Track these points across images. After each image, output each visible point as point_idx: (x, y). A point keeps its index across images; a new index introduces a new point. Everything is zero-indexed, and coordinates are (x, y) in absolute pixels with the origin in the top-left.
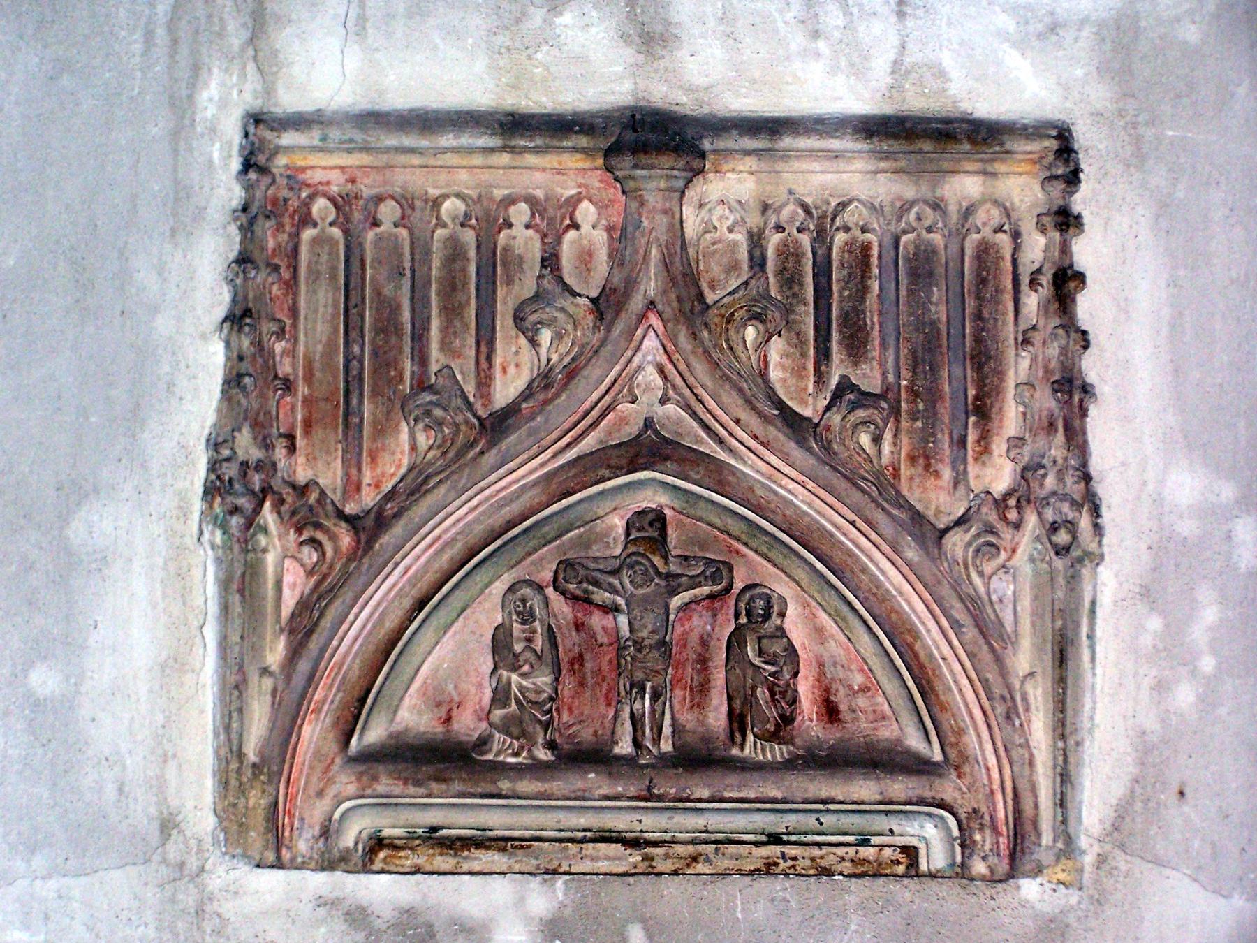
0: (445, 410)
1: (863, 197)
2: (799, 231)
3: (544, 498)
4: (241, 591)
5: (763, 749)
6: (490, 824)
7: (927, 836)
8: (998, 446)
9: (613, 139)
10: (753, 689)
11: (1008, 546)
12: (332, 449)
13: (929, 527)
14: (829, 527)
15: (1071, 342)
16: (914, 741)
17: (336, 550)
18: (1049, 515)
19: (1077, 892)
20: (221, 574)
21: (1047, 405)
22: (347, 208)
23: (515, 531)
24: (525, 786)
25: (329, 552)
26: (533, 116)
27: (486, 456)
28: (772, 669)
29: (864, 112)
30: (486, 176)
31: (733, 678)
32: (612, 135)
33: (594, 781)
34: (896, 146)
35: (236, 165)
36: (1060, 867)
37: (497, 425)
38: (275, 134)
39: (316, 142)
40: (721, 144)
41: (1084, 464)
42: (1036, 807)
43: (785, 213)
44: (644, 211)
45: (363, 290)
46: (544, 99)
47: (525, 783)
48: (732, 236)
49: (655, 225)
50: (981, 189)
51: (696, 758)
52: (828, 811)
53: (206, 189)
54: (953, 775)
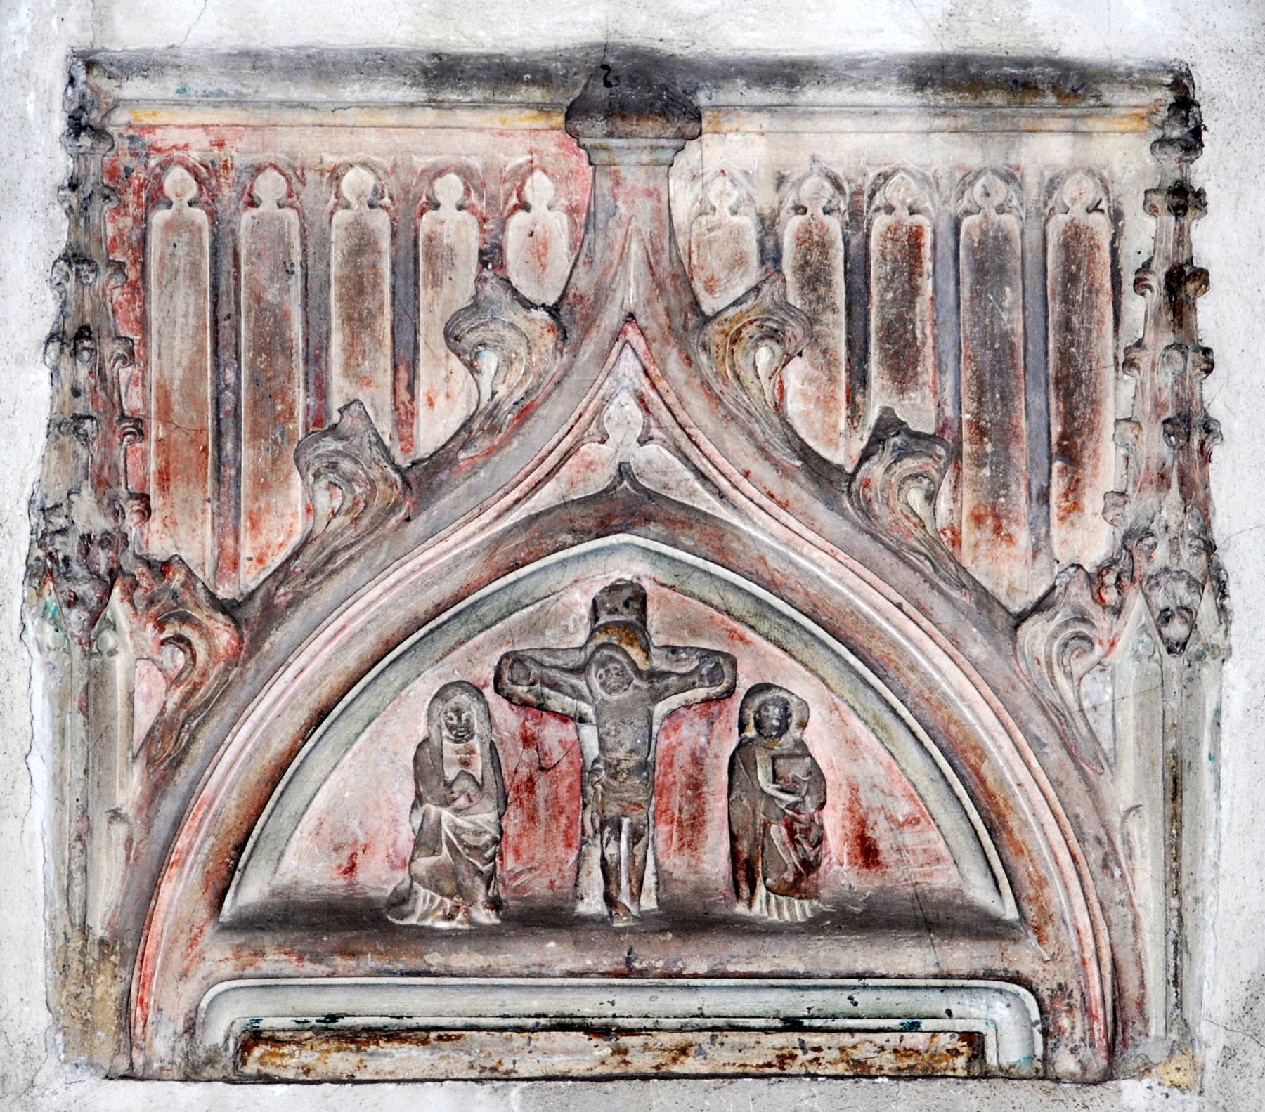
0: (357, 462)
1: (910, 166)
2: (827, 212)
3: (485, 574)
4: (84, 710)
5: (779, 906)
6: (410, 1009)
7: (997, 1019)
8: (1092, 501)
9: (577, 93)
10: (766, 826)
11: (1105, 637)
12: (199, 512)
13: (1002, 613)
14: (866, 609)
15: (1189, 365)
16: (980, 893)
17: (212, 651)
18: (1160, 599)
19: (1196, 1097)
20: (52, 685)
21: (1156, 451)
22: (214, 182)
23: (445, 616)
24: (465, 959)
25: (202, 656)
26: (468, 57)
27: (412, 525)
28: (790, 799)
29: (912, 50)
30: (403, 139)
31: (737, 812)
32: (575, 85)
33: (554, 952)
34: (956, 98)
35: (59, 124)
36: (1173, 1065)
37: (424, 479)
38: (114, 83)
39: (171, 95)
40: (722, 98)
41: (1206, 528)
42: (1142, 985)
43: (808, 187)
44: (620, 191)
45: (237, 295)
46: (481, 33)
47: (462, 956)
48: (735, 219)
49: (635, 214)
50: (1070, 153)
51: (688, 919)
52: (865, 987)
53: (19, 156)
54: (1033, 939)
